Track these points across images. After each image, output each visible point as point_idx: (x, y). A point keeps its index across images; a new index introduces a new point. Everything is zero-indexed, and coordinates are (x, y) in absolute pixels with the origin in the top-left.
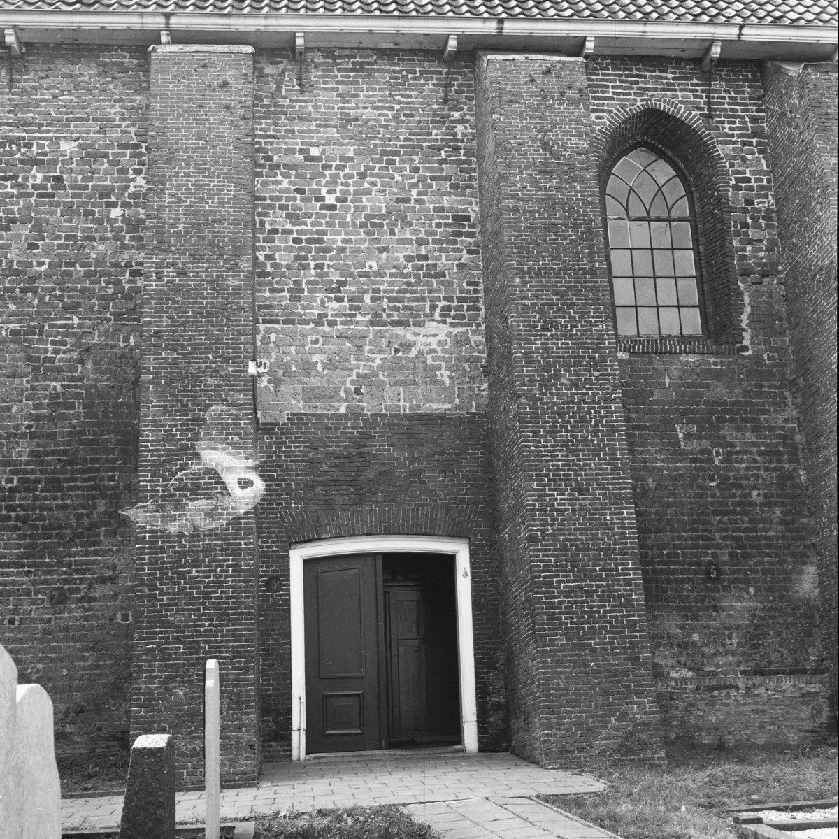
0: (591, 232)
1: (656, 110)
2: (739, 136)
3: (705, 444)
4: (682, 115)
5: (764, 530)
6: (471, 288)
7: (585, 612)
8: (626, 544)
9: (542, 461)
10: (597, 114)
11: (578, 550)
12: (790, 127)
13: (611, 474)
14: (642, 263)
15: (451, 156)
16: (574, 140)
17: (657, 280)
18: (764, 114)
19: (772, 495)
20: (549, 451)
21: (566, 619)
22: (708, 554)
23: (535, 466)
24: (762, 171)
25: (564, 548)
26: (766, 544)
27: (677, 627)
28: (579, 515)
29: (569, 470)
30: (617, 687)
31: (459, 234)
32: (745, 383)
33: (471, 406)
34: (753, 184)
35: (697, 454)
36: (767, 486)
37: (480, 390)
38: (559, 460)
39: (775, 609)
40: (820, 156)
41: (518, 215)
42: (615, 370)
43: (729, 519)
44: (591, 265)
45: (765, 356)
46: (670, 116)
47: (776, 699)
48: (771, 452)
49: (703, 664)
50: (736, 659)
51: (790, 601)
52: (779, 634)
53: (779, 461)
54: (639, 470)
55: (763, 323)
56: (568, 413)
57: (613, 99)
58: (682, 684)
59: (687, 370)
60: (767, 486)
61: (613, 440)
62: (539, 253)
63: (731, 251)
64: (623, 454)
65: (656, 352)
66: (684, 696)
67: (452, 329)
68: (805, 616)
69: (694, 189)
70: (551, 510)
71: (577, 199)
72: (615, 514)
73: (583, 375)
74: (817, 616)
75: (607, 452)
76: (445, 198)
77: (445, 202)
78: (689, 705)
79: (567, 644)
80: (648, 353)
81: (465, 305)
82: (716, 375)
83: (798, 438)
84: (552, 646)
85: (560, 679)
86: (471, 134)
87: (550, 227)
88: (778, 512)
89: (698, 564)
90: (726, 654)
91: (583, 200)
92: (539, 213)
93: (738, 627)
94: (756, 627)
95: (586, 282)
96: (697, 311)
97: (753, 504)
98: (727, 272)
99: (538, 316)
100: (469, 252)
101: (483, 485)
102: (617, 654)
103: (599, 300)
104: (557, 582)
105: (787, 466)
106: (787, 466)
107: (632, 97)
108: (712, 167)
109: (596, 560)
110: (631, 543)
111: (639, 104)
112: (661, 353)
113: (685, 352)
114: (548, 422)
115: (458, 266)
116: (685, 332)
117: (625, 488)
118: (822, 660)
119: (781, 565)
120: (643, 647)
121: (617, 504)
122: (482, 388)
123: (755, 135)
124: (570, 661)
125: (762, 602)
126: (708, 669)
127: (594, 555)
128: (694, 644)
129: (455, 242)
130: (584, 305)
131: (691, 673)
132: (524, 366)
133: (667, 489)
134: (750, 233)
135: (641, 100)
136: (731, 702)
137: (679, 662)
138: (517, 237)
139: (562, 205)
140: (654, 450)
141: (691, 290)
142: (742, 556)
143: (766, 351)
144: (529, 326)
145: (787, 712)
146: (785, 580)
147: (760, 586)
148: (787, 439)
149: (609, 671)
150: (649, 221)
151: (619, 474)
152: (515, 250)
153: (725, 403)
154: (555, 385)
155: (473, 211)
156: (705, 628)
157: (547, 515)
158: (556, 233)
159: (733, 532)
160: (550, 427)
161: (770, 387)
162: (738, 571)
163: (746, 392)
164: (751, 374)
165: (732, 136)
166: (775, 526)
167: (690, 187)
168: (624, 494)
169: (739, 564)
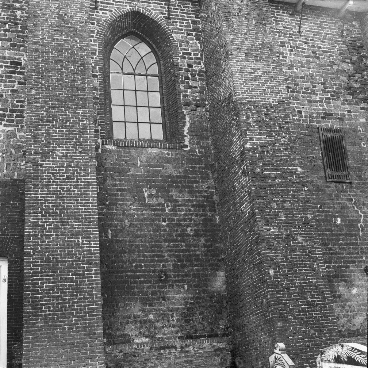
0: (84, 67)
1: (138, 12)
2: (185, 30)
3: (161, 200)
4: (153, 16)
5: (195, 251)
6: (19, 104)
7: (59, 303)
8: (92, 257)
9: (38, 203)
10: (103, 11)
11: (57, 261)
12: (211, 23)
13: (85, 212)
14: (130, 98)
15: (12, 28)
16: (78, 14)
17: (138, 108)
18: (199, 20)
19: (199, 231)
20: (44, 197)
21: (45, 308)
22: (160, 265)
23: (33, 206)
24: (198, 50)
25: (48, 260)
26: (195, 259)
27: (140, 310)
28: (61, 238)
29: (56, 209)
30: (78, 354)
31: (14, 72)
32: (185, 166)
33: (14, 175)
34: (192, 56)
35: (156, 206)
36: (197, 225)
37: (20, 165)
38: (50, 203)
39: (200, 298)
40: (225, 34)
41: (38, 53)
42: (93, 148)
43: (174, 245)
44: (83, 85)
45: (197, 151)
46: (147, 16)
47: (200, 353)
48: (199, 205)
49: (155, 333)
50: (176, 329)
51: (209, 293)
52: (201, 313)
53: (204, 210)
54: (120, 215)
55: (197, 132)
56: (59, 173)
57: (113, 4)
58: (141, 347)
59: (151, 157)
60: (197, 225)
61: (88, 191)
62: (49, 76)
63: (179, 92)
64: (94, 200)
65: (133, 147)
66: (142, 354)
67: (5, 128)
68: (218, 302)
69: (161, 59)
70: (41, 236)
71: (77, 47)
72: (85, 238)
73: (71, 150)
74: (225, 302)
75: (83, 198)
76: (7, 51)
77: (7, 53)
78: (146, 360)
79: (44, 326)
80: (128, 147)
81: (15, 114)
82: (168, 161)
83: (215, 197)
84: (34, 327)
85: (38, 350)
86: (26, 16)
87: (58, 62)
88: (203, 240)
89: (154, 271)
90: (170, 326)
91: (81, 49)
92: (52, 53)
93: (177, 310)
94: (188, 309)
95: (78, 95)
96: (161, 126)
97: (188, 235)
98: (176, 103)
99: (45, 113)
100: (19, 83)
101: (18, 223)
102: (79, 331)
103: (86, 106)
104: (41, 283)
105: (208, 213)
106: (208, 213)
107: (125, 4)
108: (169, 46)
109: (70, 268)
110: (94, 257)
111: (128, 8)
112: (136, 147)
113: (150, 147)
114: (45, 179)
115: (12, 91)
116: (153, 138)
117: (93, 221)
118: (228, 328)
119: (204, 271)
120: (98, 326)
121: (87, 231)
122: (22, 164)
123: (194, 30)
124: (45, 337)
125: (192, 294)
126: (158, 336)
127: (68, 265)
128: (150, 321)
129: (11, 77)
130: (76, 109)
131: (147, 339)
132: (32, 144)
133: (136, 226)
134: (190, 83)
135: (130, 6)
136: (172, 356)
137: (140, 333)
138: (35, 66)
139: (67, 50)
140: (129, 203)
141: (157, 115)
142: (181, 266)
143: (198, 148)
144: (39, 119)
145: (206, 361)
146: (206, 280)
147: (191, 285)
148: (209, 198)
149: (73, 343)
150: (135, 75)
151: (90, 212)
152: (33, 74)
153: (173, 176)
154: (52, 155)
155: (24, 59)
156: (157, 310)
157: (38, 239)
158: (61, 66)
159: (176, 252)
160: (46, 182)
161: (199, 168)
162: (178, 275)
163: (186, 171)
164: (189, 161)
165: (182, 30)
166: (200, 248)
167: (159, 58)
168: (92, 225)
169: (179, 271)
